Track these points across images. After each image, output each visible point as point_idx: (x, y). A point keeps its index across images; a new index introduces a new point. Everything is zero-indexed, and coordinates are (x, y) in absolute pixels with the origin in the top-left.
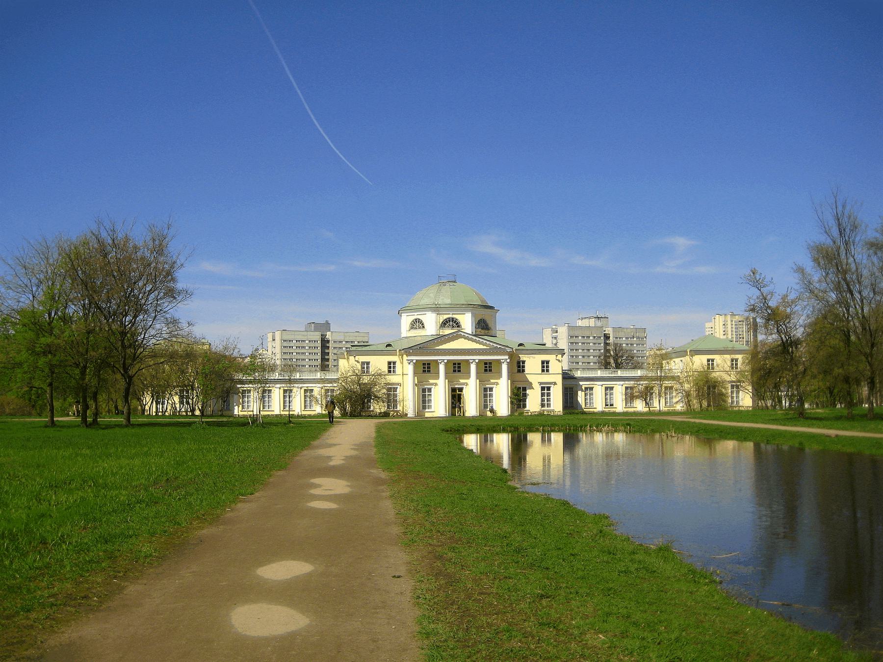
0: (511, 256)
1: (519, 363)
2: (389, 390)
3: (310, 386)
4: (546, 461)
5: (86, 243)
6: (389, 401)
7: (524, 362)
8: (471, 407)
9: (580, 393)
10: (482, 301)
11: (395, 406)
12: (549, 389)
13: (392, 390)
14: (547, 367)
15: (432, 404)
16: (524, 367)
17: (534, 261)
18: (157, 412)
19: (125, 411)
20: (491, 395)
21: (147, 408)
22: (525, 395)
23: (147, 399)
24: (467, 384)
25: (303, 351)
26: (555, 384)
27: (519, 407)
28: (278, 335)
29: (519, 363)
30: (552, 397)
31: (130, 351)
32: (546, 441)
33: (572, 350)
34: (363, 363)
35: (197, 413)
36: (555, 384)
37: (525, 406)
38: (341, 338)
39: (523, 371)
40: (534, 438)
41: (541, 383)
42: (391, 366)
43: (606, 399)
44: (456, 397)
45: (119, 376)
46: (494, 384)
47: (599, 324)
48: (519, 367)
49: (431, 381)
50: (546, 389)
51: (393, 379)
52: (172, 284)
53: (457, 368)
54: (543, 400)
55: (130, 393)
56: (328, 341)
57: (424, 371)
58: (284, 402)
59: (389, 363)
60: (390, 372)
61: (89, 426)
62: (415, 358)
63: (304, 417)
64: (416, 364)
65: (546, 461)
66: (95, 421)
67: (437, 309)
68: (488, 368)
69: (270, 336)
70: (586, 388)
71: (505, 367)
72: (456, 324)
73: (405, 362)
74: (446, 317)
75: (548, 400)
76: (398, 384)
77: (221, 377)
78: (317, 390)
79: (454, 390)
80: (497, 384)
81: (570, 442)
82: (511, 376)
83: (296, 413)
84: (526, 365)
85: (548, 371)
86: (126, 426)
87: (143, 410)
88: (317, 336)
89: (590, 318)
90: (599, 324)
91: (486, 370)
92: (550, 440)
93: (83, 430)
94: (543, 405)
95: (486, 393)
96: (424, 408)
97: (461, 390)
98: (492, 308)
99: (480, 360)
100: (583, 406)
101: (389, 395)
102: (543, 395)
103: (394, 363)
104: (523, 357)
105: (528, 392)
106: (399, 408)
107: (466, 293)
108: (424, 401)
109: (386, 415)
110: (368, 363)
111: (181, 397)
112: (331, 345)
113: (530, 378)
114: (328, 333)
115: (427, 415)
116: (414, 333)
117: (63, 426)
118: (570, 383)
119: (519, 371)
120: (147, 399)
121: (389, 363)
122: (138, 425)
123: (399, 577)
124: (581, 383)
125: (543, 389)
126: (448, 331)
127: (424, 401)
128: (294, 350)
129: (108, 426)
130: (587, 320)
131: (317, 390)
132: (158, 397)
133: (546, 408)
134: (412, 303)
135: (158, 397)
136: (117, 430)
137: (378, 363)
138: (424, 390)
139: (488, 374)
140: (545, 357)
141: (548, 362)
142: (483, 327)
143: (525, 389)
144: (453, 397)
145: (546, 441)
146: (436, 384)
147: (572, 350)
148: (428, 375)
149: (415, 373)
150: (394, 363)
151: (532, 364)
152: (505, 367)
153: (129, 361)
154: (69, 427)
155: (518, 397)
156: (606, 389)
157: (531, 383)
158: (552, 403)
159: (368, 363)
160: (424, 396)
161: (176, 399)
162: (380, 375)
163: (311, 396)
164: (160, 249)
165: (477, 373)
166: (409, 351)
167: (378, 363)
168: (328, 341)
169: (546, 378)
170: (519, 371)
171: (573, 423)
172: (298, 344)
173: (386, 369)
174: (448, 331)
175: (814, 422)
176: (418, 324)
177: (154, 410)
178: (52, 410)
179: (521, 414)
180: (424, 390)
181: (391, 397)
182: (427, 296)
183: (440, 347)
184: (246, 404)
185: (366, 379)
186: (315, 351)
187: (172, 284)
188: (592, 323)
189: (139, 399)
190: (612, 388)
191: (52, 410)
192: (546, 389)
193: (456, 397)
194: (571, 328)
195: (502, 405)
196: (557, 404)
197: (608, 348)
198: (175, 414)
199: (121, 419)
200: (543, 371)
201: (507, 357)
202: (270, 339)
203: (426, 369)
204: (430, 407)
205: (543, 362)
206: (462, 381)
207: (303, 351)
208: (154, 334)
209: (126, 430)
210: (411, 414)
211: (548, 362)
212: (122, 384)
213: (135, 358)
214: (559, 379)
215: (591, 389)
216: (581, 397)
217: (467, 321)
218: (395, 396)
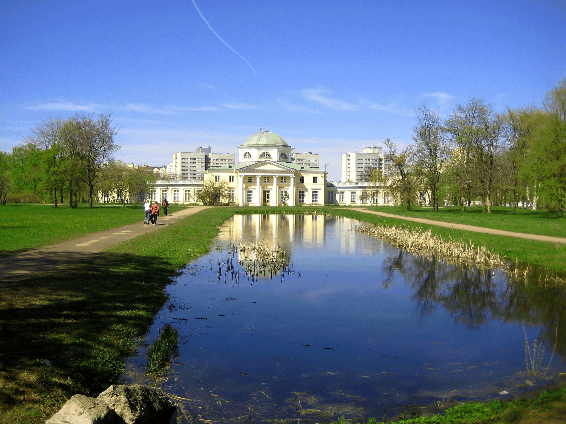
0: (331, 103)
1: (301, 178)
2: (230, 191)
3: (177, 188)
4: (314, 229)
5: (71, 123)
6: (230, 197)
7: (303, 177)
9: (337, 194)
10: (284, 143)
11: (233, 200)
12: (317, 192)
13: (231, 191)
15: (253, 199)
17: (346, 107)
18: (105, 201)
19: (90, 201)
21: (100, 199)
22: (304, 195)
23: (100, 194)
24: (272, 189)
25: (194, 165)
26: (320, 189)
27: (300, 202)
28: (179, 155)
29: (301, 178)
30: (318, 197)
31: (92, 174)
32: (314, 219)
33: (358, 167)
34: (216, 177)
35: (126, 202)
36: (320, 189)
37: (303, 201)
38: (218, 157)
39: (303, 182)
40: (308, 218)
44: (266, 196)
45: (86, 185)
47: (376, 151)
49: (252, 187)
50: (315, 192)
51: (231, 185)
52: (112, 144)
53: (266, 180)
54: (313, 198)
55: (92, 192)
56: (210, 159)
58: (174, 197)
59: (230, 177)
60: (230, 181)
61: (73, 207)
62: (244, 174)
63: (351, 207)
64: (245, 177)
65: (314, 229)
66: (75, 206)
67: (258, 147)
68: (283, 180)
70: (341, 192)
71: (292, 180)
73: (239, 176)
77: (141, 182)
78: (192, 190)
79: (264, 191)
81: (329, 222)
82: (296, 185)
83: (180, 203)
84: (305, 179)
86: (91, 208)
87: (98, 201)
88: (203, 156)
89: (370, 148)
90: (376, 151)
91: (282, 182)
92: (316, 219)
93: (71, 209)
94: (313, 201)
96: (248, 201)
97: (268, 192)
98: (290, 147)
101: (230, 194)
102: (313, 195)
103: (233, 177)
104: (303, 175)
105: (305, 193)
106: (235, 201)
107: (274, 138)
108: (248, 198)
109: (228, 204)
110: (219, 177)
111: (118, 194)
112: (211, 161)
113: (306, 186)
114: (210, 155)
115: (250, 205)
116: (246, 160)
117: (61, 208)
118: (331, 189)
120: (100, 194)
121: (230, 177)
123: (219, 278)
124: (338, 189)
125: (313, 192)
126: (263, 159)
127: (248, 198)
128: (189, 165)
129: (81, 208)
130: (369, 149)
131: (192, 190)
132: (105, 193)
134: (246, 143)
135: (105, 194)
136: (87, 209)
137: (224, 177)
138: (248, 192)
139: (283, 184)
140: (315, 175)
141: (316, 178)
142: (284, 157)
143: (303, 192)
144: (264, 195)
145: (314, 219)
147: (358, 167)
149: (244, 182)
150: (233, 177)
151: (308, 179)
153: (91, 178)
155: (301, 195)
156: (352, 193)
159: (219, 177)
160: (248, 195)
161: (115, 195)
162: (225, 183)
163: (189, 194)
164: (105, 126)
165: (277, 183)
167: (224, 177)
168: (210, 159)
169: (315, 186)
170: (301, 182)
171: (332, 209)
172: (192, 161)
173: (228, 180)
174: (263, 159)
176: (247, 155)
177: (103, 200)
178: (56, 200)
179: (301, 205)
180: (248, 192)
181: (231, 196)
182: (254, 141)
183: (257, 169)
184: (153, 198)
185: (217, 185)
186: (202, 165)
187: (112, 144)
188: (372, 151)
189: (95, 195)
191: (56, 200)
192: (315, 192)
193: (266, 196)
194: (358, 154)
195: (256, 201)
196: (321, 201)
197: (381, 166)
198: (114, 202)
199: (88, 205)
200: (314, 182)
203: (250, 180)
204: (251, 201)
205: (314, 178)
206: (269, 187)
207: (194, 165)
208: (103, 161)
209: (90, 210)
210: (241, 204)
211: (316, 178)
212: (88, 188)
213: (94, 176)
214: (322, 187)
215: (343, 192)
216: (337, 197)
217: (274, 154)
218: (233, 194)
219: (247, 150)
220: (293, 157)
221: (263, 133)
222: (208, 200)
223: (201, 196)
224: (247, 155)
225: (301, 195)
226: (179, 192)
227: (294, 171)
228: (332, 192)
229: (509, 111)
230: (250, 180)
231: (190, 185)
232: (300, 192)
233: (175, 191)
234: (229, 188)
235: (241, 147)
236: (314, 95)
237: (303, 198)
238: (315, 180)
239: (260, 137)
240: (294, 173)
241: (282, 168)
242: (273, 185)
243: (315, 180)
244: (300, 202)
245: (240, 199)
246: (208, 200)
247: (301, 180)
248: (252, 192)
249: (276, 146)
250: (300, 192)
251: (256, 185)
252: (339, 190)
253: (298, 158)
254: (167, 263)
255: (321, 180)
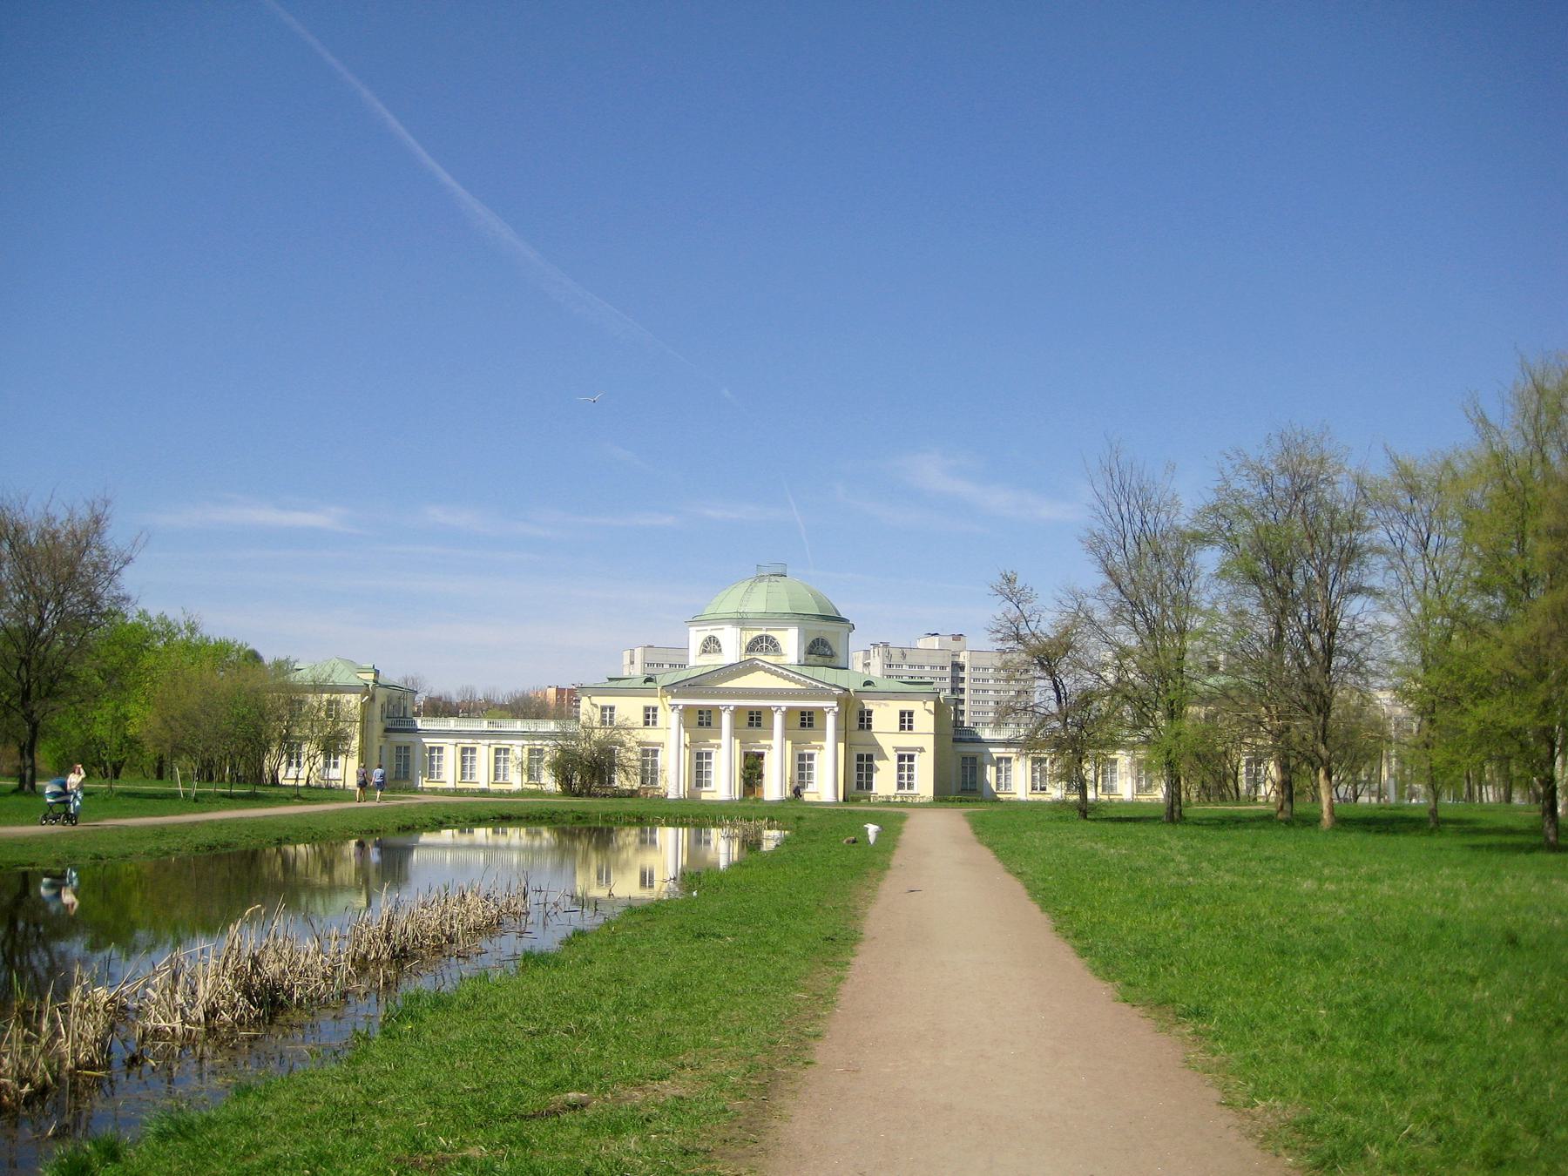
2: (645, 753)
3: (504, 743)
7: (870, 713)
8: (773, 788)
12: (911, 758)
13: (649, 753)
14: (910, 721)
15: (712, 779)
16: (870, 720)
20: (810, 767)
22: (871, 768)
26: (922, 750)
28: (638, 652)
29: (861, 713)
30: (915, 773)
34: (604, 709)
36: (922, 750)
37: (870, 786)
39: (869, 727)
41: (897, 749)
42: (650, 716)
43: (1033, 778)
46: (712, 746)
48: (862, 720)
50: (906, 759)
51: (651, 735)
54: (900, 777)
57: (701, 724)
60: (647, 723)
62: (682, 702)
67: (741, 621)
69: (627, 654)
70: (1000, 759)
71: (830, 720)
72: (771, 645)
74: (756, 634)
75: (910, 777)
76: (659, 744)
80: (821, 748)
82: (844, 734)
85: (910, 728)
91: (803, 725)
94: (901, 786)
95: (803, 765)
96: (699, 784)
98: (840, 620)
99: (789, 709)
100: (994, 787)
101: (644, 763)
102: (901, 768)
103: (655, 709)
104: (869, 705)
108: (699, 773)
109: (632, 794)
110: (612, 709)
115: (705, 796)
118: (970, 749)
119: (861, 727)
121: (647, 709)
122: (1252, 820)
125: (901, 758)
127: (699, 773)
132: (293, 756)
133: (906, 791)
137: (629, 709)
138: (699, 756)
140: (906, 705)
142: (819, 651)
143: (870, 758)
146: (821, 748)
148: (758, 730)
150: (655, 709)
151: (884, 716)
152: (830, 720)
154: (1120, 820)
157: (880, 749)
158: (915, 782)
159: (612, 709)
166: (673, 689)
167: (629, 709)
168: (962, 668)
169: (906, 740)
170: (861, 727)
173: (641, 720)
175: (1152, 814)
176: (711, 645)
180: (699, 756)
181: (649, 771)
182: (730, 601)
190: (506, 751)
192: (906, 759)
195: (722, 785)
200: (902, 728)
201: (834, 704)
202: (627, 661)
203: (703, 720)
204: (708, 784)
205: (902, 714)
211: (911, 714)
214: (929, 743)
216: (991, 774)
217: (790, 642)
218: (654, 763)
219: (709, 631)
220: (961, 660)
221: (761, 578)
222: (577, 781)
223: (562, 769)
224: (711, 645)
225: (861, 767)
226: (916, 763)
227: (838, 692)
228: (974, 759)
229: (1396, 462)
230: (703, 720)
231: (543, 736)
232: (860, 757)
233: (464, 750)
234: (640, 744)
235: (698, 621)
236: (931, 471)
237: (870, 777)
238: (906, 720)
239: (749, 591)
240: (838, 699)
241: (797, 682)
242: (771, 737)
243: (906, 720)
244: (860, 786)
245: (672, 780)
246: (577, 781)
247: (865, 720)
248: (709, 755)
249: (797, 617)
250: (860, 757)
251: (823, 738)
252: (997, 752)
253: (975, 663)
254: (1474, 847)
255: (925, 720)
